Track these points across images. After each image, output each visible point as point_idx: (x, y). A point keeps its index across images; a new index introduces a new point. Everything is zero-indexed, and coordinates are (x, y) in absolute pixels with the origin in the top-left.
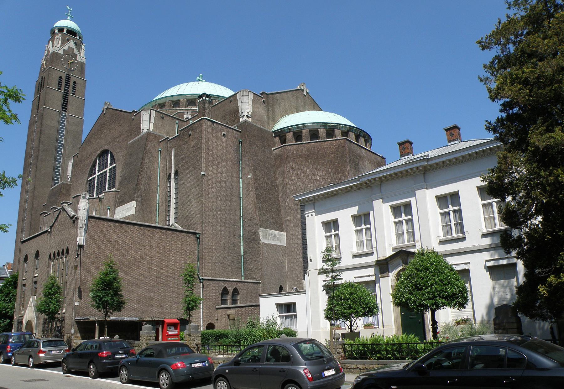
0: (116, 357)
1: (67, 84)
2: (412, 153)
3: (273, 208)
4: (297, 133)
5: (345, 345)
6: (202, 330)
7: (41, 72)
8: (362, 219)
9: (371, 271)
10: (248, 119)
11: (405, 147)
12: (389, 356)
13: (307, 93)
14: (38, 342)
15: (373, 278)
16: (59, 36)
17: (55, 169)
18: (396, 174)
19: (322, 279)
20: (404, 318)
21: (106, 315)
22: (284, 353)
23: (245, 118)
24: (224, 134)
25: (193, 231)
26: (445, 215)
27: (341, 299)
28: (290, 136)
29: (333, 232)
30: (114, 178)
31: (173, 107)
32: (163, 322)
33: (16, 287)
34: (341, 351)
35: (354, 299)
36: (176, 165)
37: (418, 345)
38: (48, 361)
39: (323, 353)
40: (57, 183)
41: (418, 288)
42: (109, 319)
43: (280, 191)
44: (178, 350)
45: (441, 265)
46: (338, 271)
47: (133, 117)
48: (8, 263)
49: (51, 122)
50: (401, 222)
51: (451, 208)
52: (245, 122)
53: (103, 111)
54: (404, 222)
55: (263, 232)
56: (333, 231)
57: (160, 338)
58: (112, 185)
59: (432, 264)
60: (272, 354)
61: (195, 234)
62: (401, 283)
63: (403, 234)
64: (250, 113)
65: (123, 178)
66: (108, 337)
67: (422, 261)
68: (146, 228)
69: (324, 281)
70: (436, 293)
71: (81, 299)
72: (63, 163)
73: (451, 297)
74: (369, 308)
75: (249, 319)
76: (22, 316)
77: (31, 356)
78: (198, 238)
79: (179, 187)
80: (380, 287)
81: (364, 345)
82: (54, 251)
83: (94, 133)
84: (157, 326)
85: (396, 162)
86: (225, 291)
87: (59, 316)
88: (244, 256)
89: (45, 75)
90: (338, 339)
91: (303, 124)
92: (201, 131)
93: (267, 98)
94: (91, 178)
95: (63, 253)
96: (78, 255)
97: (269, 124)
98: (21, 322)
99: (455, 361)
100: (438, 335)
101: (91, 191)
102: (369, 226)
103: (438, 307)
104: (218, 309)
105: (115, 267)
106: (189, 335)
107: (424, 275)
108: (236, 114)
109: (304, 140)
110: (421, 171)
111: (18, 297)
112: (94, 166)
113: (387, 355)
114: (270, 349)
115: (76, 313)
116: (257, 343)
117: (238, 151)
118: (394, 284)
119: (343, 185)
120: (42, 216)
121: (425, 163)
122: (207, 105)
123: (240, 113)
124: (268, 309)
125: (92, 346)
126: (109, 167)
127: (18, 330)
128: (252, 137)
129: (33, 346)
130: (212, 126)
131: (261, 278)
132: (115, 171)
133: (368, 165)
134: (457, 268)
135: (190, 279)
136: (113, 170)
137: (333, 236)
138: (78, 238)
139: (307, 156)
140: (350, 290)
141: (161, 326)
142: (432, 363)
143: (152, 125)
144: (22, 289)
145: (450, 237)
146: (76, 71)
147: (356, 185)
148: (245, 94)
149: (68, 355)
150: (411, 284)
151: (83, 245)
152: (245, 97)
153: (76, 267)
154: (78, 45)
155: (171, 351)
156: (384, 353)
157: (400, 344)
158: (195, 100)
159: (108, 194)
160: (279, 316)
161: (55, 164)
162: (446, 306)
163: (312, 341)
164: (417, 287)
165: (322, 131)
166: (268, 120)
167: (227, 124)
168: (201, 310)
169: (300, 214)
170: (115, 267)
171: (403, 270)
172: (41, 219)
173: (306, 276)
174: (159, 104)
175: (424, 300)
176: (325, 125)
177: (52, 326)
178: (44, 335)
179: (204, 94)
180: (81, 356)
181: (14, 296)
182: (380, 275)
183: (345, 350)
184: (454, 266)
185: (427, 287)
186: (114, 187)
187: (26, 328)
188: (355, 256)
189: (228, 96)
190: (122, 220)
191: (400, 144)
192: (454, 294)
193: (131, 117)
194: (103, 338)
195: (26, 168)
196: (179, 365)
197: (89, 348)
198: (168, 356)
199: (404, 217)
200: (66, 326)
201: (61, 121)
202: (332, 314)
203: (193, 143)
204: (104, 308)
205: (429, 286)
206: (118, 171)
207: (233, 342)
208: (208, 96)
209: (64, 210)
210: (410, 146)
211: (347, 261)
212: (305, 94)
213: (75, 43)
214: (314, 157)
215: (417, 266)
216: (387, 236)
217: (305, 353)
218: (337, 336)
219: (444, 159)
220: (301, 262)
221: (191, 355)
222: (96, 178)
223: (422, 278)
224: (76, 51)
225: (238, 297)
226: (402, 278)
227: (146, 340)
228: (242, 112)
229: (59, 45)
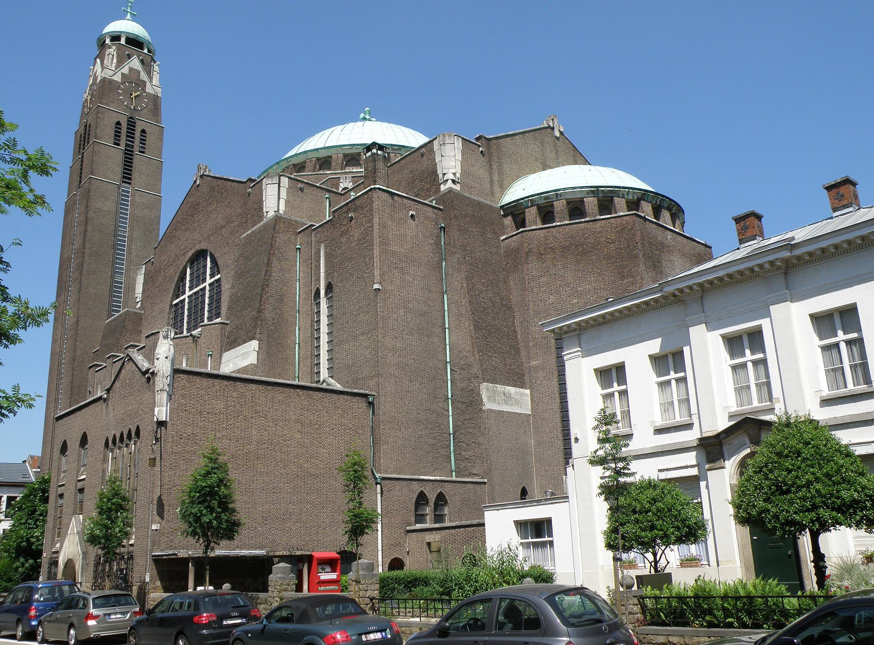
0: (225, 623)
1: (131, 134)
2: (761, 234)
3: (503, 347)
4: (545, 207)
5: (643, 598)
6: (380, 570)
7: (83, 115)
8: (669, 361)
9: (691, 458)
10: (454, 186)
11: (748, 224)
12: (730, 620)
13: (561, 133)
14: (85, 599)
15: (694, 472)
16: (113, 50)
17: (113, 285)
18: (730, 276)
19: (597, 475)
20: (756, 546)
21: (207, 547)
22: (528, 613)
24: (412, 216)
25: (362, 391)
26: (831, 349)
27: (634, 512)
28: (531, 214)
29: (616, 387)
30: (219, 300)
31: (320, 169)
32: (310, 558)
33: (46, 500)
34: (637, 609)
35: (659, 510)
36: (327, 274)
37: (786, 600)
38: (103, 634)
39: (602, 613)
40: (118, 311)
41: (781, 489)
42: (212, 555)
43: (517, 315)
44: (337, 609)
45: (825, 446)
46: (624, 459)
47: (250, 190)
48: (32, 457)
49: (104, 204)
50: (744, 365)
51: (841, 336)
52: (450, 191)
54: (750, 365)
55: (487, 389)
56: (615, 384)
57: (305, 587)
58: (215, 312)
59: (807, 444)
60: (506, 615)
61: (365, 396)
62: (747, 481)
63: (748, 387)
64: (458, 175)
65: (234, 299)
66: (211, 588)
67: (786, 438)
69: (602, 478)
70: (818, 500)
71: (162, 517)
72: (128, 276)
73: (850, 506)
74: (688, 527)
75: (466, 550)
76: (57, 552)
77: (71, 626)
78: (371, 404)
79: (335, 312)
80: (707, 487)
81: (681, 598)
82: (113, 432)
83: (178, 223)
84: (300, 565)
85: (729, 253)
86: (422, 499)
87: (123, 550)
88: (454, 433)
89: (90, 120)
90: (630, 587)
91: (556, 190)
92: (371, 210)
93: (488, 147)
94: (178, 300)
95: (129, 437)
96: (157, 439)
97: (492, 193)
98: (55, 563)
99: (862, 635)
100: (828, 582)
101: (177, 324)
102: (682, 374)
103: (824, 527)
104: (409, 531)
105: (221, 459)
106: (356, 581)
107: (792, 465)
108: (432, 177)
109: (557, 219)
110: (779, 268)
111: (50, 519)
112: (182, 278)
113: (726, 617)
114: (504, 605)
115: (154, 543)
116: (482, 594)
117: (438, 244)
118: (735, 481)
119: (631, 300)
120: (92, 370)
121: (786, 254)
122: (380, 165)
123: (441, 176)
124: (500, 530)
125: (181, 604)
126: (209, 281)
127: (49, 578)
128: (463, 219)
129: (76, 606)
131: (486, 474)
132: (219, 286)
133: (678, 261)
134: (860, 451)
135: (356, 477)
136: (216, 286)
137: (617, 395)
138: (156, 409)
140: (650, 493)
141: (306, 565)
142: (812, 636)
144: (56, 502)
145: (842, 392)
146: (145, 111)
147: (655, 300)
148: (447, 141)
149: (139, 622)
150: (767, 483)
152: (448, 147)
153: (152, 462)
155: (324, 611)
156: (720, 614)
157: (750, 598)
158: (359, 154)
159: (209, 328)
160: (522, 544)
161: (112, 277)
162: (841, 524)
163: (580, 591)
164: (779, 488)
165: (591, 203)
166: (492, 186)
167: (417, 196)
168: (380, 533)
169: (554, 355)
170: (221, 459)
171: (752, 455)
172: (90, 376)
173: (569, 470)
174: (294, 165)
175: (795, 513)
176: (595, 191)
177: (111, 568)
178: (96, 586)
179: (374, 144)
180: (163, 622)
181: (44, 514)
182: (707, 466)
183: (644, 608)
184: (852, 448)
185: (800, 488)
186: (218, 315)
187: (63, 574)
188: (659, 431)
189: (417, 146)
190: (234, 375)
191: (738, 220)
192: (855, 502)
193: (246, 190)
194: (202, 588)
195: (62, 287)
196: (339, 637)
197: (177, 607)
198: (319, 620)
199: (749, 356)
200: (136, 569)
201: (121, 201)
202: (618, 540)
203: (356, 234)
204: (205, 535)
205: (803, 486)
206: (225, 287)
207: (438, 593)
208: (381, 147)
209: (131, 359)
210: (756, 222)
211: (643, 439)
212: (557, 134)
213: (142, 62)
214: (576, 250)
215: (779, 448)
216: (717, 393)
217: (566, 614)
218: (629, 581)
219: (823, 244)
220: (560, 444)
221: (361, 617)
222: (187, 301)
223: (789, 471)
224: (143, 76)
225: (446, 510)
226: (750, 471)
227: (280, 592)
228: (444, 174)
229: (114, 65)
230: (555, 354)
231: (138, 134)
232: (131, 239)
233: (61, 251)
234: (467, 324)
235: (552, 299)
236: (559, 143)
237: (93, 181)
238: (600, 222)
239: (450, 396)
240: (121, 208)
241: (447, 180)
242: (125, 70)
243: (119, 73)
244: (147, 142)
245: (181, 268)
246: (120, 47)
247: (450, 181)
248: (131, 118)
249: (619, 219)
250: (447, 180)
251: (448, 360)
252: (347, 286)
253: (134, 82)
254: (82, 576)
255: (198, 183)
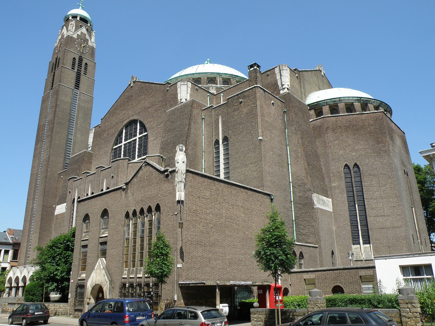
4: (333, 106)
7: (54, 53)
23: (286, 90)
24: (273, 103)
25: (268, 193)
28: (326, 109)
43: (322, 160)
48: (10, 230)
53: (130, 85)
61: (269, 195)
68: (233, 187)
71: (183, 261)
78: (272, 200)
88: (295, 221)
91: (339, 98)
92: (255, 97)
93: (299, 74)
94: (117, 146)
98: (81, 286)
130: (264, 94)
138: (177, 194)
139: (347, 128)
143: (189, 95)
146: (87, 54)
151: (182, 201)
154: (89, 31)
161: (67, 136)
165: (357, 105)
176: (359, 99)
201: (74, 98)
212: (323, 75)
213: (87, 30)
214: (353, 128)
224: (87, 37)
229: (73, 30)
230: (344, 181)
231: (83, 65)
234: (302, 162)
235: (341, 152)
236: (324, 79)
237: (60, 86)
238: (364, 115)
239: (292, 200)
240: (73, 101)
241: (285, 88)
243: (76, 34)
245: (120, 129)
246: (77, 22)
247: (286, 89)
248: (81, 56)
249: (375, 114)
250: (285, 88)
251: (291, 181)
252: (239, 138)
253: (83, 39)
254: (109, 294)
255: (132, 85)
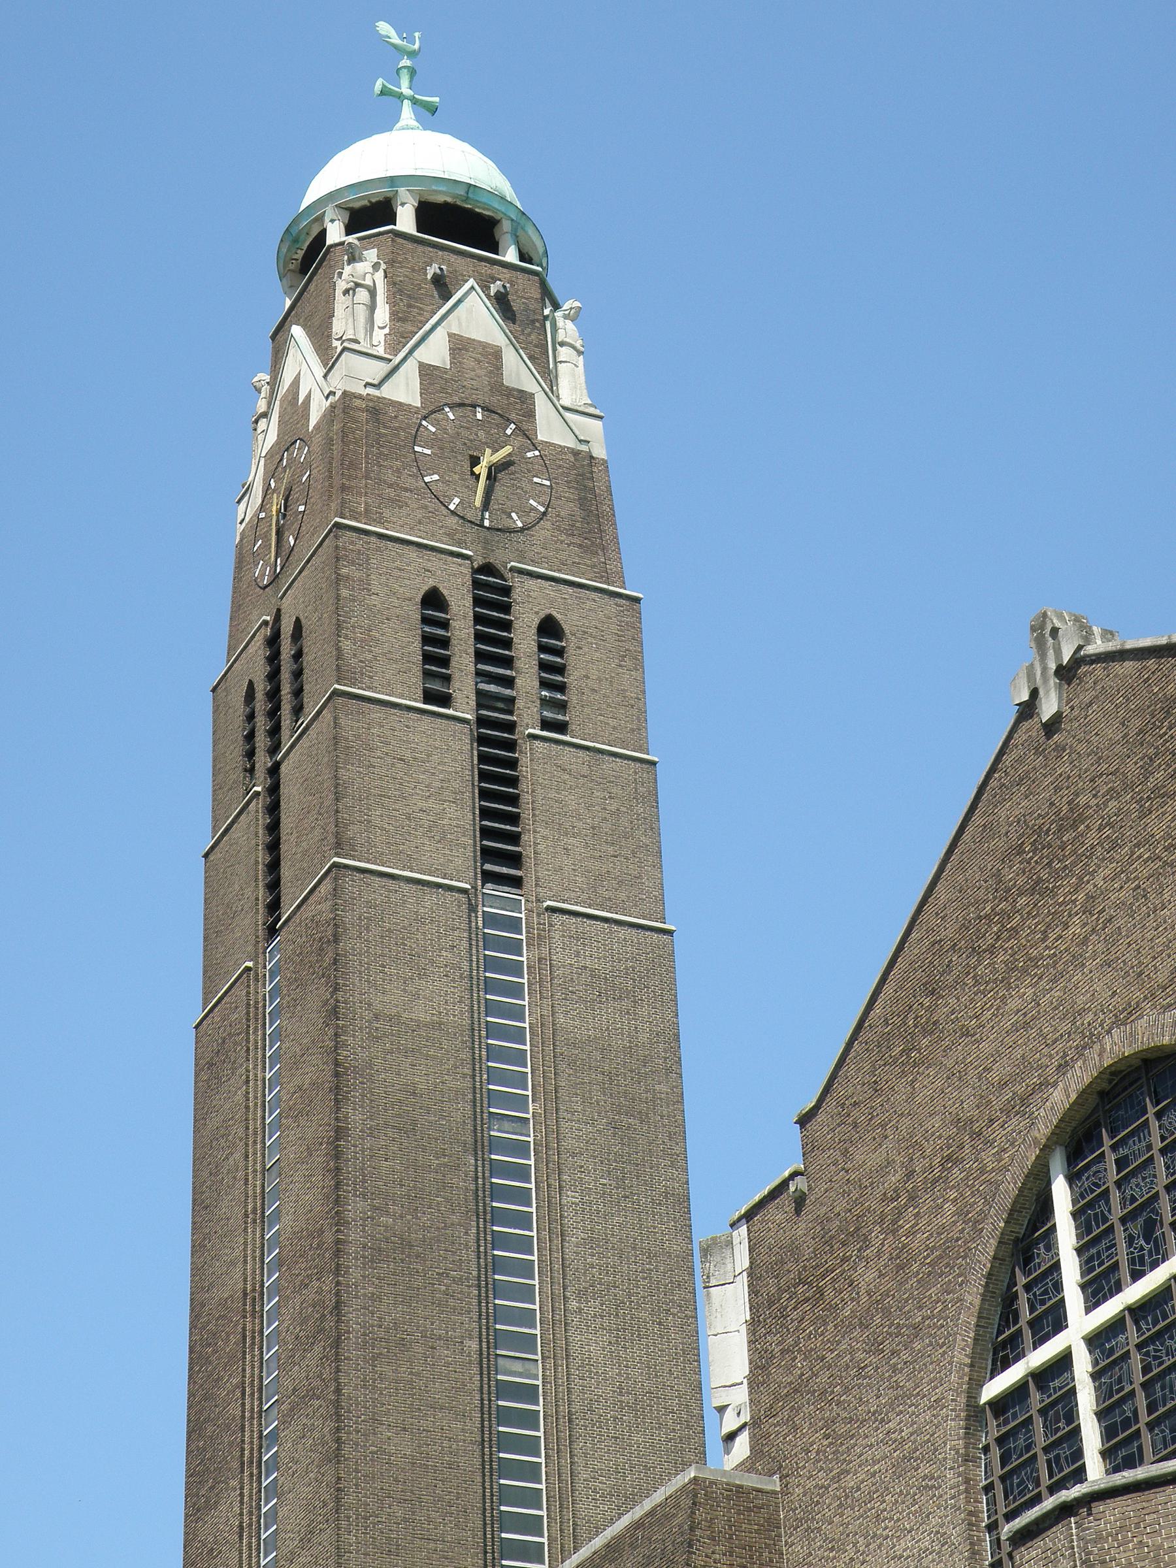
49: (413, 982)
53: (1028, 709)
146: (543, 532)
154: (526, 312)
161: (486, 1364)
201: (492, 966)
213: (502, 303)
224: (517, 371)
229: (379, 336)
231: (525, 642)
232: (551, 1148)
233: (197, 1271)
237: (351, 884)
242: (435, 351)
243: (411, 367)
244: (572, 678)
253: (481, 403)
255: (1049, 707)
